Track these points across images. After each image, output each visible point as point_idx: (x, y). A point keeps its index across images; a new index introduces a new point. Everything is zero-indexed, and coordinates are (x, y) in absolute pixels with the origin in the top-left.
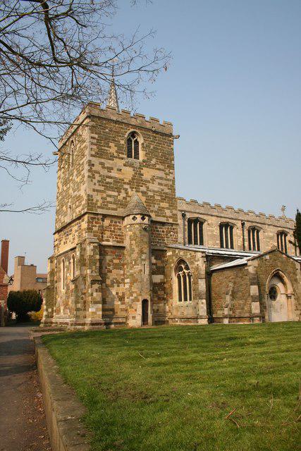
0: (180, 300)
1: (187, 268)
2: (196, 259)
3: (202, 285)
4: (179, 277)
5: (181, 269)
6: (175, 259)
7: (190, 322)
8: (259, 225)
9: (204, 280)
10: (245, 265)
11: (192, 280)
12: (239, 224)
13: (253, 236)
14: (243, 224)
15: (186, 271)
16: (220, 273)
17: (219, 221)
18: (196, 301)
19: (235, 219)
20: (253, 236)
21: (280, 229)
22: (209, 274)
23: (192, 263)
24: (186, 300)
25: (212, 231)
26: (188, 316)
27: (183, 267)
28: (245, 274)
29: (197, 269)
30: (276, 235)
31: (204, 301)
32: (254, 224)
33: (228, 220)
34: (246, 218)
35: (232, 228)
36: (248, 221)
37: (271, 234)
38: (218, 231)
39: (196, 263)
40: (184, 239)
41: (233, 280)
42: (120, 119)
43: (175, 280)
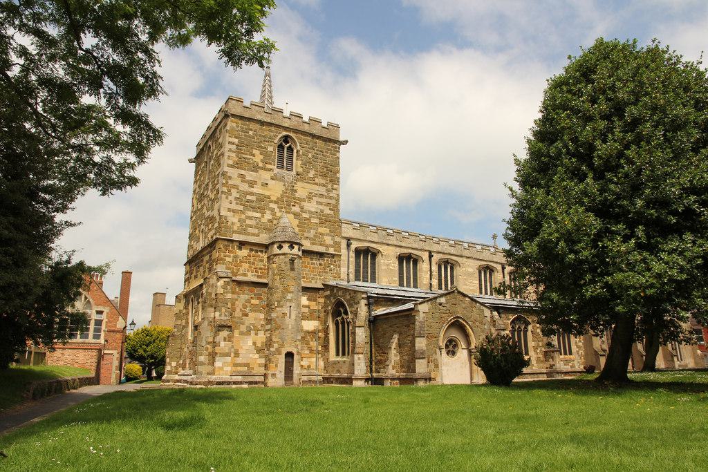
12: (425, 256)
14: (431, 256)
19: (421, 250)
33: (410, 251)
37: (471, 270)
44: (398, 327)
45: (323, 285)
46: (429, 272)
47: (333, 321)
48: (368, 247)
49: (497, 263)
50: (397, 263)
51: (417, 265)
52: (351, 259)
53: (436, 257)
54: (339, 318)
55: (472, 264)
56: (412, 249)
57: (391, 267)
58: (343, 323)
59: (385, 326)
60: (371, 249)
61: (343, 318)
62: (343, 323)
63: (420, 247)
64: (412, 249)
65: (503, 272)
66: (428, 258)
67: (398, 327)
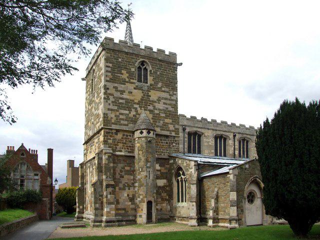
1: (184, 174)
3: (193, 190)
4: (178, 182)
5: (179, 175)
9: (195, 185)
11: (187, 185)
12: (231, 136)
13: (243, 145)
15: (183, 177)
19: (228, 132)
20: (243, 145)
22: (200, 181)
24: (186, 202)
26: (184, 216)
27: (181, 173)
32: (245, 136)
33: (222, 133)
35: (225, 139)
38: (213, 142)
41: (218, 186)
43: (175, 183)
44: (217, 184)
53: (238, 136)
58: (182, 181)
62: (182, 181)
65: (234, 138)
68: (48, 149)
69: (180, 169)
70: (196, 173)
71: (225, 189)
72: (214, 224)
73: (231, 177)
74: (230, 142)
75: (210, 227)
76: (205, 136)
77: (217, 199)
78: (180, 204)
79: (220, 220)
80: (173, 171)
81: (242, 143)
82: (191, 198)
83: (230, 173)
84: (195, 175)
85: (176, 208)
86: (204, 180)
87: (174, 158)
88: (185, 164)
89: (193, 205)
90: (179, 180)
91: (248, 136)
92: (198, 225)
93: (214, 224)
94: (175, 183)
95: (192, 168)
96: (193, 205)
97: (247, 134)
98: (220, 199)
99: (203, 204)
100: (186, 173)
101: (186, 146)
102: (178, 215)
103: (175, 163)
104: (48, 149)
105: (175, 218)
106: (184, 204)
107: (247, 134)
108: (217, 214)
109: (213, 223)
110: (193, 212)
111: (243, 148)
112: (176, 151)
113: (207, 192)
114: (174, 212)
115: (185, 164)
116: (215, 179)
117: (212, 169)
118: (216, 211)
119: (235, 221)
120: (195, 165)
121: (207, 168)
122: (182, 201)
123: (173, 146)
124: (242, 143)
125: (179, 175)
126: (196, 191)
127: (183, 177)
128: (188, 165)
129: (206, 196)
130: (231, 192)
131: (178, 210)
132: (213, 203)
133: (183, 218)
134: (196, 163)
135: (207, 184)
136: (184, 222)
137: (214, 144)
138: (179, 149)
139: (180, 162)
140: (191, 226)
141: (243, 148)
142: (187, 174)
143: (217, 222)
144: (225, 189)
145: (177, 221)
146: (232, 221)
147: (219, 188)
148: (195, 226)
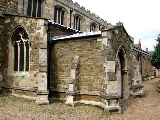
0: (16, 69)
1: (26, 37)
2: (37, 27)
3: (43, 55)
4: (16, 46)
5: (18, 38)
6: (13, 27)
7: (26, 94)
8: (81, 15)
9: (46, 50)
10: (99, 36)
11: (30, 49)
12: (69, 11)
13: (77, 22)
14: (71, 11)
15: (24, 40)
16: (63, 44)
17: (56, 3)
18: (34, 73)
19: (67, 6)
20: (77, 22)
21: (92, 21)
22: (51, 45)
23: (32, 31)
24: (27, 70)
25: (49, 11)
26: (24, 88)
27: (21, 35)
28: (97, 46)
29: (38, 38)
30: (90, 25)
31: (45, 74)
32: (79, 13)
33: (61, 5)
34: (74, 7)
35: (63, 12)
36: (75, 10)
37: (88, 24)
38: (53, 12)
39: (37, 31)
40: (23, 11)
41: (79, 53)
42: (23, 91)
43: (11, 48)
44: (78, 51)
45: (4, 14)
46: (70, 21)
47: (12, 44)
48: (61, 6)
49: (97, 22)
50: (54, 11)
51: (63, 14)
52: (72, 22)
53: (74, 13)
54: (18, 41)
55: (88, 21)
56: (63, 4)
57: (50, 13)
58: (22, 46)
59: (63, 49)
60: (63, 9)
61: (22, 41)
62: (22, 46)
63: (66, 4)
64: (63, 4)
65: (71, 13)
66: (70, 12)
67: (78, 51)
68: (33, 81)
69: (20, 29)
70: (46, 35)
71: (91, 56)
72: (76, 102)
73: (105, 41)
74: (67, 16)
75: (71, 106)
76: (46, 3)
77: (78, 69)
78: (18, 73)
79: (82, 97)
80: (9, 33)
81: (76, 19)
82: (39, 66)
83: (103, 35)
84: (44, 38)
85: (12, 78)
86: (56, 45)
87: (12, 17)
88: (29, 24)
89: (43, 77)
90: (18, 44)
91: (81, 15)
92: (51, 103)
93: (76, 102)
94: (11, 48)
95: (40, 28)
96: (43, 77)
97: (80, 13)
98: (81, 70)
99: (53, 74)
100: (29, 35)
101: (26, 9)
102: (15, 86)
103: (13, 22)
104: (33, 81)
105: (10, 90)
106: (24, 73)
107: (80, 13)
108: (78, 89)
109: (74, 101)
110: (43, 87)
111: (77, 25)
112: (14, 11)
113: (59, 61)
114: (9, 82)
115: (29, 24)
116: (74, 44)
117: (63, 34)
118: (77, 84)
119: (115, 101)
120: (45, 25)
121: (58, 31)
122: (22, 70)
123: (10, 4)
124: (76, 19)
125: (18, 38)
126: (46, 57)
127: (24, 40)
128: (34, 25)
129: (59, 65)
130: (109, 61)
131: (16, 80)
132: (73, 73)
133: (23, 91)
134: (46, 23)
135: (59, 49)
136: (24, 96)
137: (53, 14)
138: (17, 9)
139: (21, 21)
140: (40, 104)
141: (77, 25)
142: (31, 37)
143: (78, 99)
144: (91, 56)
145: (13, 94)
146: (111, 101)
147: (82, 56)
148: (45, 104)
